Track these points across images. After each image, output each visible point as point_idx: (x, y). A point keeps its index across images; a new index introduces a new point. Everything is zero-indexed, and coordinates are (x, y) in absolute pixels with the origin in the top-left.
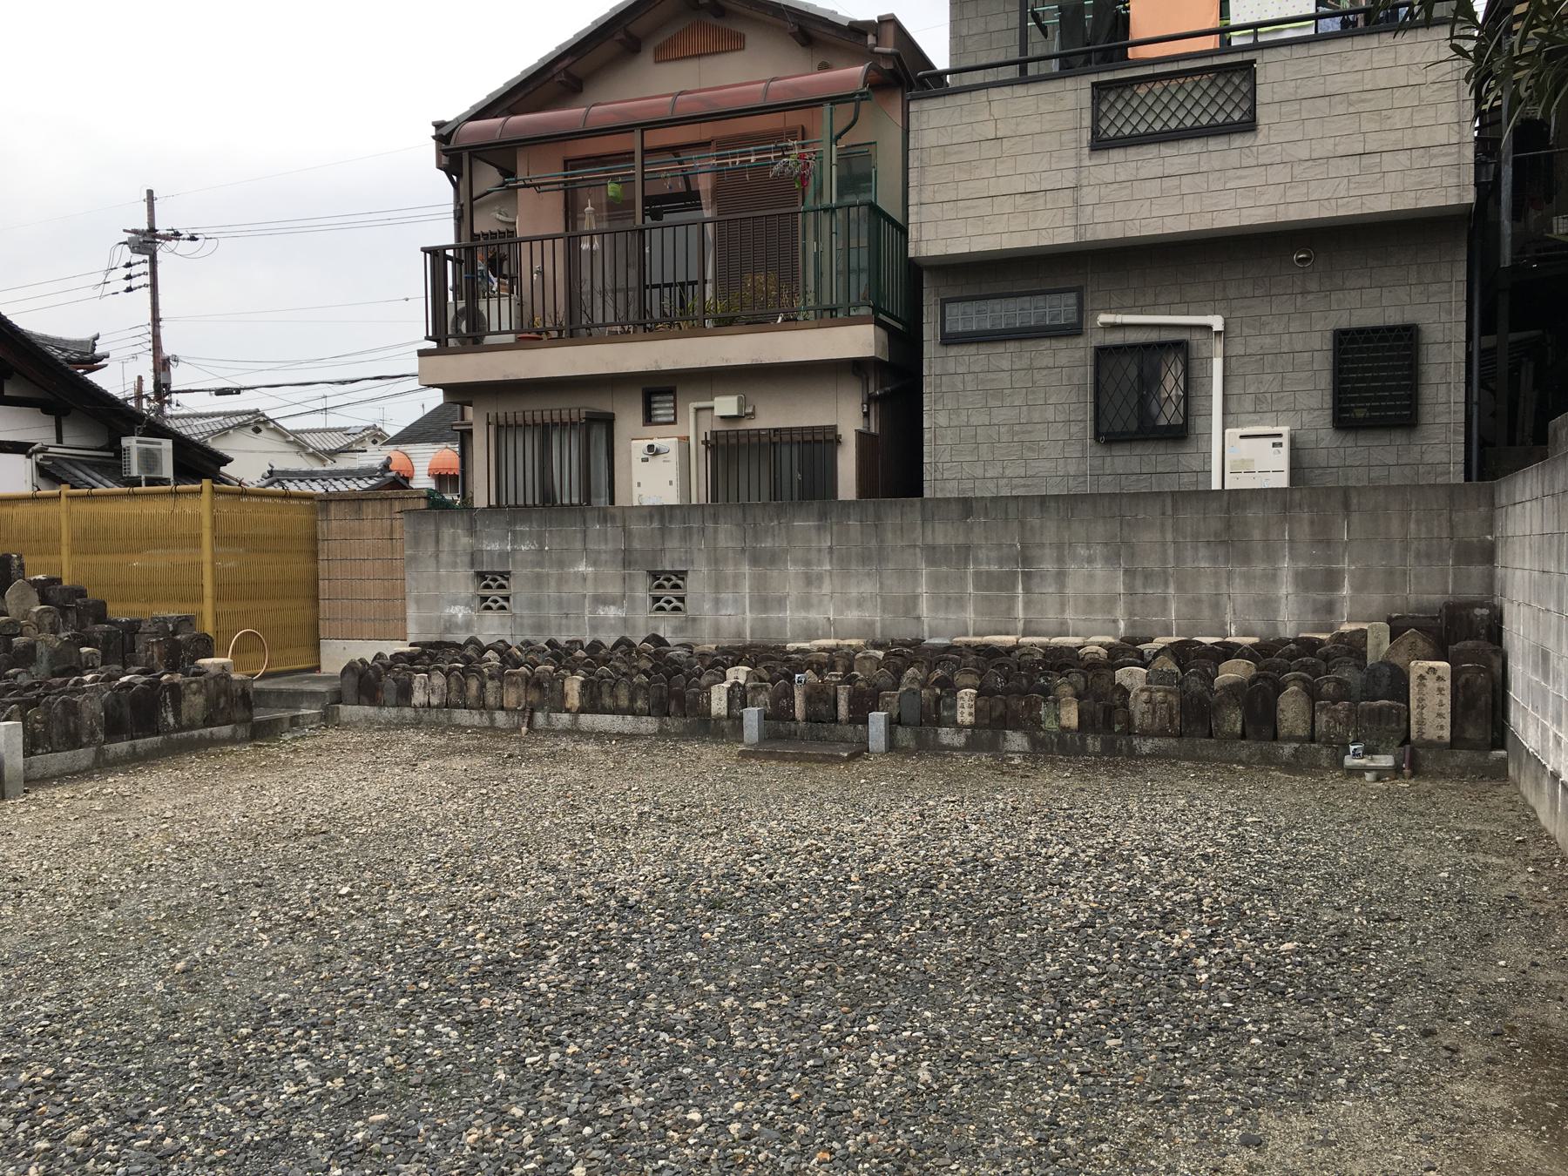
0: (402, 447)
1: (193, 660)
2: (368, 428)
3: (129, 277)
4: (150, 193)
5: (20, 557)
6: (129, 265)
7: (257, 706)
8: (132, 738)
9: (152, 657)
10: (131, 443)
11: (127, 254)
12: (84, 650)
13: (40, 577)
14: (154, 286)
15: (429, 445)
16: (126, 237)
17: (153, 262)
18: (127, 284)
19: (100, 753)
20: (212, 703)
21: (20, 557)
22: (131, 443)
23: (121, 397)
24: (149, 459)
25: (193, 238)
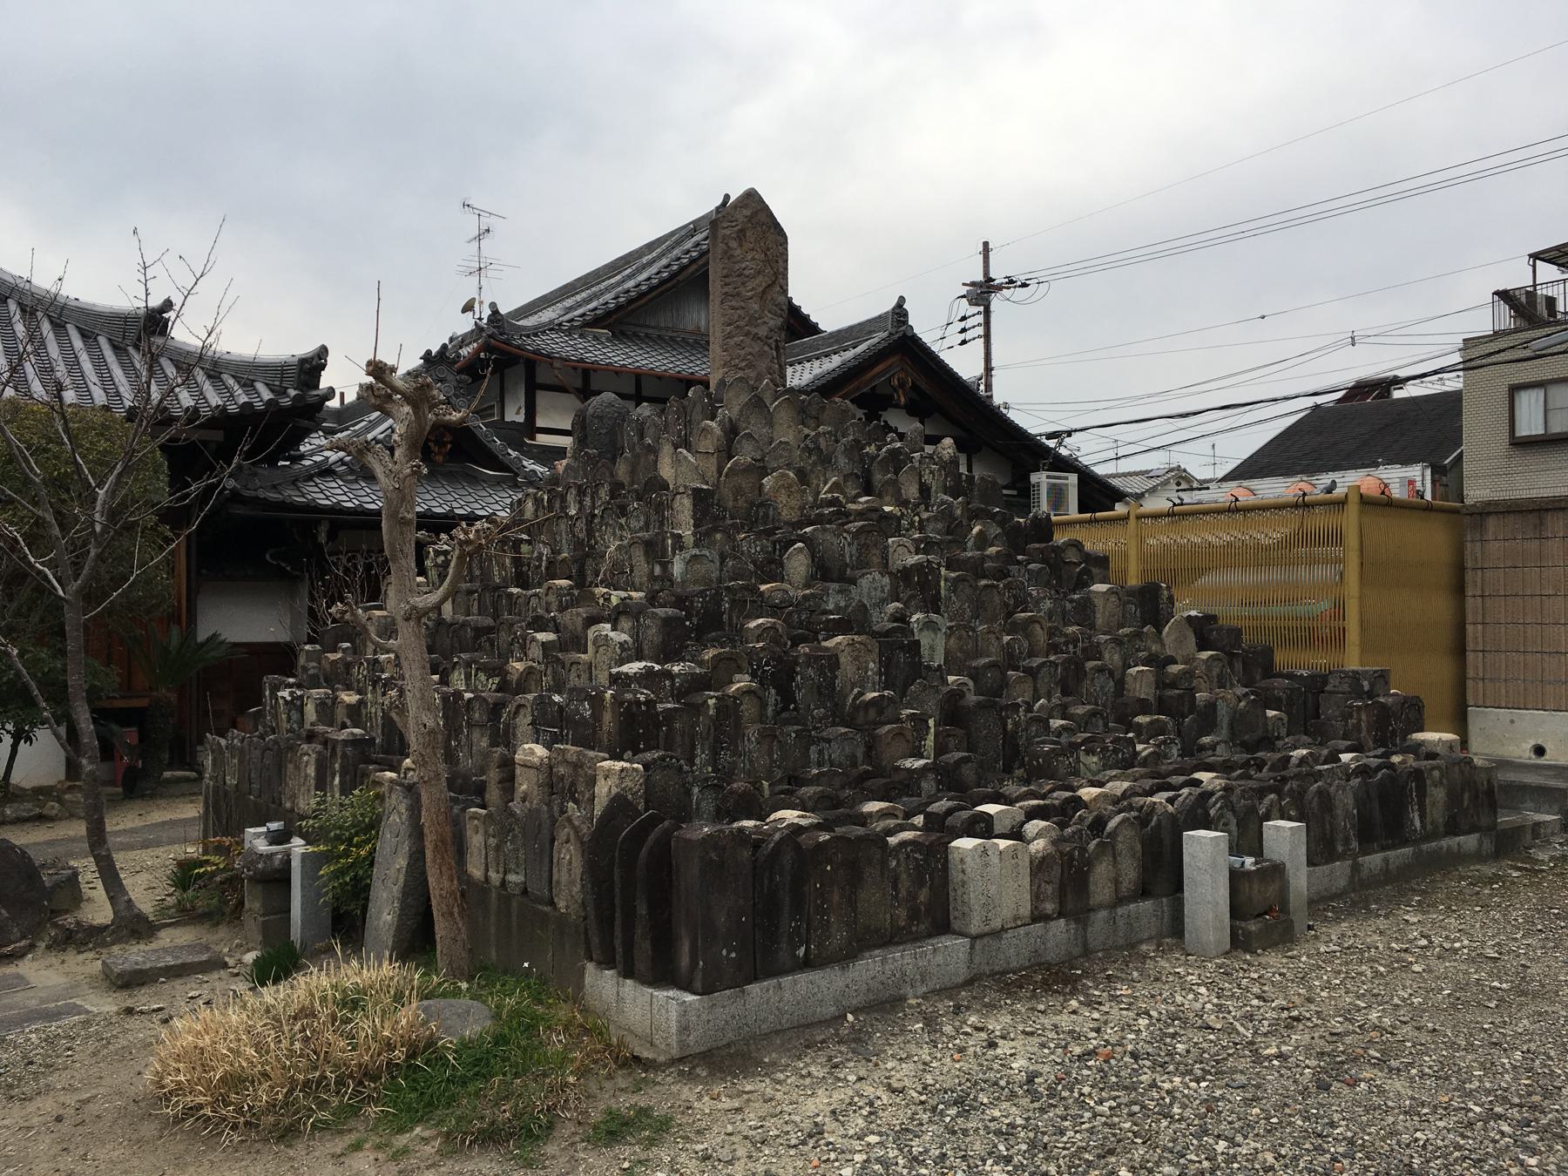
0: (1246, 483)
1: (1404, 739)
2: (1171, 470)
3: (963, 330)
4: (986, 244)
5: (1169, 588)
6: (964, 318)
7: (1502, 807)
8: (1383, 849)
9: (1358, 727)
10: (1041, 479)
11: (965, 307)
12: (1271, 713)
13: (1193, 613)
14: (987, 337)
15: (1281, 479)
16: (964, 290)
17: (987, 313)
18: (962, 336)
19: (1356, 868)
20: (1454, 797)
21: (1169, 588)
22: (1041, 479)
23: (1032, 431)
24: (1057, 496)
25: (1024, 285)
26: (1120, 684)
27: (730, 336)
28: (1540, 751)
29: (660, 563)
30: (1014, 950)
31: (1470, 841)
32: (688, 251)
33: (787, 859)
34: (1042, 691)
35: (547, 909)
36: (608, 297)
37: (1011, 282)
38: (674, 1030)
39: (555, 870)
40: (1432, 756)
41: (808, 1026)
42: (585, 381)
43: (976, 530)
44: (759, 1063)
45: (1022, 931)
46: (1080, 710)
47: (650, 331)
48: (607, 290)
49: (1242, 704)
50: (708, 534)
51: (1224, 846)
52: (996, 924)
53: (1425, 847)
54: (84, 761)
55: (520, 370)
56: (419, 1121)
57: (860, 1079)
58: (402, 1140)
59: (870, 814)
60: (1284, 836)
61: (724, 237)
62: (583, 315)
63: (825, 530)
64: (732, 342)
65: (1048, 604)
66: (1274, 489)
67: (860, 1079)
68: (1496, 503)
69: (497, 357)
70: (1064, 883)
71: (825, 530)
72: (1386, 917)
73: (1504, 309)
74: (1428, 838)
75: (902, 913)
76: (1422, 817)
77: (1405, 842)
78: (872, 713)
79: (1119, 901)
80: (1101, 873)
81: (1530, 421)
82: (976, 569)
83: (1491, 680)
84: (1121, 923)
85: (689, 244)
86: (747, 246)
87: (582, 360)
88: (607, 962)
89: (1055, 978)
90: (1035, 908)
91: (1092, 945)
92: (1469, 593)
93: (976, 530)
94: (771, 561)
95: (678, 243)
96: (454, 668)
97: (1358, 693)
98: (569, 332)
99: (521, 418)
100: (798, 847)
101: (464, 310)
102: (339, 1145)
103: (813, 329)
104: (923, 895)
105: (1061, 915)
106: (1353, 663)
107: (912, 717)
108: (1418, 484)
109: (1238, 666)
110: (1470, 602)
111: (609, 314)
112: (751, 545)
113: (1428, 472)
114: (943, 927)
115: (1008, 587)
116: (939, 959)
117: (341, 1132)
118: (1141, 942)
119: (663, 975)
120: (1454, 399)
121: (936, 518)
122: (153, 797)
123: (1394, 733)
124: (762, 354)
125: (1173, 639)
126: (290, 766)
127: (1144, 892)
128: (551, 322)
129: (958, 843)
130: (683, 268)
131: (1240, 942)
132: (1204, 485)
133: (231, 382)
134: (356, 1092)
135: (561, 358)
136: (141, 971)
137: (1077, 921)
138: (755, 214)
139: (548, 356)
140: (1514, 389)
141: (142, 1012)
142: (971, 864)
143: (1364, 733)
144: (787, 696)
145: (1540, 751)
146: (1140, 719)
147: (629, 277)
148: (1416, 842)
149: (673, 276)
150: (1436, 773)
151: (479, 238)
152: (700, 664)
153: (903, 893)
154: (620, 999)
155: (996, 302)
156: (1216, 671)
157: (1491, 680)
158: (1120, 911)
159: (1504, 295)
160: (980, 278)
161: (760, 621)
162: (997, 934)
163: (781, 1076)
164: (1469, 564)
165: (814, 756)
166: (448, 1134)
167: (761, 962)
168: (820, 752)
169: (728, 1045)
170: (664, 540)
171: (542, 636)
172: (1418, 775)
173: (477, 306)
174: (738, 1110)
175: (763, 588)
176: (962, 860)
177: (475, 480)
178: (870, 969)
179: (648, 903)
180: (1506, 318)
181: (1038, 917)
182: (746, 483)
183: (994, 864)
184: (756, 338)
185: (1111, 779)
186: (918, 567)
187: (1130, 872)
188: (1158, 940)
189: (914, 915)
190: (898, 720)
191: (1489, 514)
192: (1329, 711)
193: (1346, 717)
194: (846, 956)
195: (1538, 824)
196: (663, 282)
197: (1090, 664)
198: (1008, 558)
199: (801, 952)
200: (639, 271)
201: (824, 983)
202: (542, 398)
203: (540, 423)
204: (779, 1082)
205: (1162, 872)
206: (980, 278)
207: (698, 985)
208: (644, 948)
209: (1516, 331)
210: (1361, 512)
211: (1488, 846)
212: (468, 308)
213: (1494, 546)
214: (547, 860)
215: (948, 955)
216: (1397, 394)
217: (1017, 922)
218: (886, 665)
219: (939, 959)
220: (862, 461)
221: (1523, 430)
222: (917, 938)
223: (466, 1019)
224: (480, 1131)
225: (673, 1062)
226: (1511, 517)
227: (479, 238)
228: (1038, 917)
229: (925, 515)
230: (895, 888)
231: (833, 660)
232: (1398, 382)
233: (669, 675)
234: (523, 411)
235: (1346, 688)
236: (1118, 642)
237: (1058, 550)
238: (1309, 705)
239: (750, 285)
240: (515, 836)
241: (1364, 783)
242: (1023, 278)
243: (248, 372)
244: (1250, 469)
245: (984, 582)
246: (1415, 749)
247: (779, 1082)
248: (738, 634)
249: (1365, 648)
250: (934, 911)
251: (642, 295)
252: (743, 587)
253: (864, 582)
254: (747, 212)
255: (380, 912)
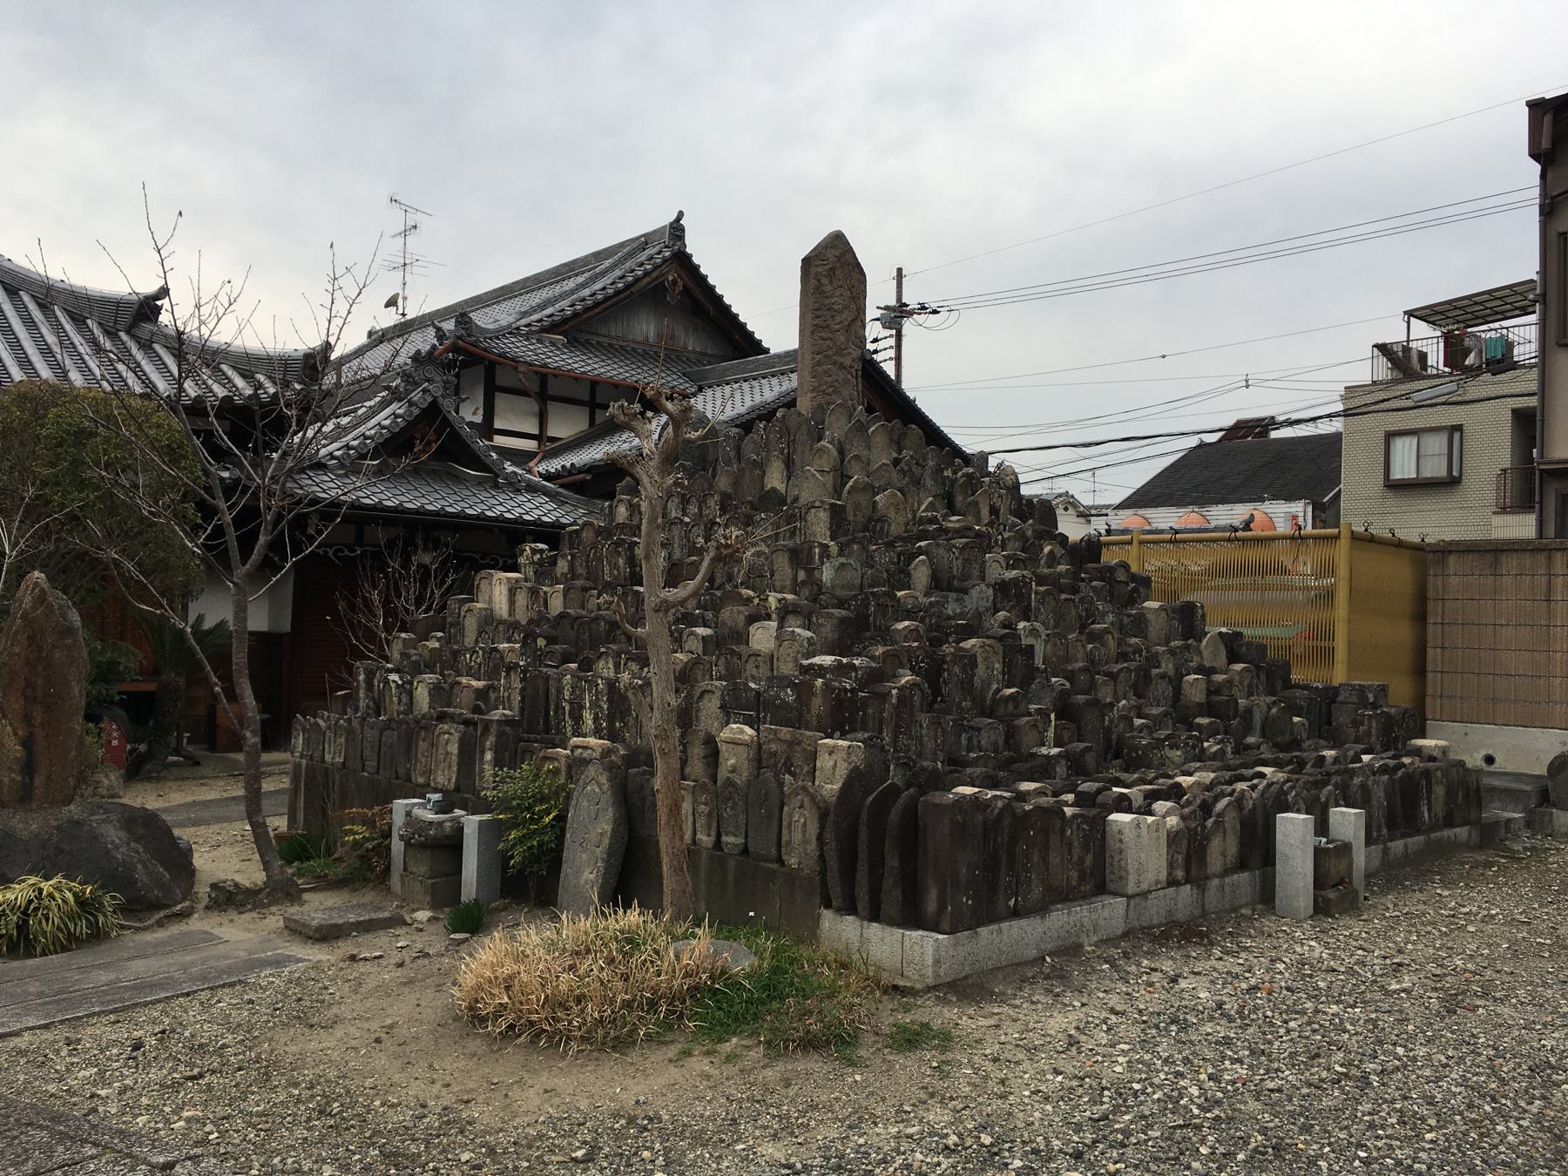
0: (1141, 512)
1: (1404, 744)
4: (900, 270)
8: (1403, 836)
9: (1368, 734)
12: (1296, 719)
13: (1224, 630)
15: (1173, 509)
17: (899, 336)
19: (1386, 851)
20: (1450, 794)
25: (935, 312)
26: (1178, 690)
27: (819, 364)
28: (1490, 760)
29: (806, 569)
30: (1154, 911)
31: (1462, 832)
32: (642, 264)
33: (1007, 822)
34: (1120, 694)
35: (775, 866)
36: (564, 303)
37: (923, 308)
38: (929, 960)
39: (785, 832)
40: (1432, 759)
41: (1018, 965)
42: (545, 390)
43: (1047, 549)
44: (992, 993)
45: (1161, 893)
46: (1155, 711)
47: (602, 339)
48: (563, 296)
49: (1274, 710)
50: (848, 544)
51: (1311, 826)
52: (1145, 886)
53: (1432, 835)
54: (248, 734)
55: (480, 371)
56: (734, 1033)
57: (1083, 1005)
58: (726, 1047)
59: (1028, 792)
60: (1347, 821)
61: (816, 274)
62: (540, 320)
63: (938, 545)
64: (820, 369)
65: (1110, 618)
66: (1165, 518)
67: (1083, 1005)
68: (1458, 543)
69: (461, 354)
70: (1189, 852)
71: (938, 545)
72: (1421, 891)
73: (1383, 362)
74: (1434, 828)
75: (1074, 874)
76: (1429, 810)
77: (1418, 832)
78: (1010, 707)
79: (1227, 872)
80: (1215, 844)
81: (1404, 465)
82: (1053, 581)
83: (1449, 697)
84: (1227, 890)
85: (643, 257)
86: (836, 283)
87: (545, 366)
88: (850, 908)
89: (1187, 933)
90: (1169, 874)
91: (1209, 907)
92: (1431, 620)
93: (1047, 549)
94: (901, 571)
95: (630, 255)
96: (599, 657)
97: (1364, 704)
98: (527, 337)
99: (478, 419)
100: (1014, 814)
101: (387, 305)
102: (672, 1051)
103: (756, 347)
104: (1089, 860)
105: (1187, 881)
106: (1339, 676)
107: (1039, 711)
108: (1301, 520)
109: (1263, 677)
110: (1431, 628)
111: (565, 320)
112: (884, 558)
113: (1310, 509)
114: (1101, 889)
115: (1082, 600)
116: (1106, 913)
117: (665, 1043)
118: (1241, 907)
119: (913, 919)
120: (1336, 438)
121: (1014, 538)
122: (158, 779)
123: (1396, 738)
124: (846, 382)
125: (1209, 650)
126: (422, 745)
127: (1242, 865)
128: (510, 325)
129: (1114, 817)
130: (637, 280)
131: (1322, 909)
132: (1101, 511)
133: (230, 372)
134: (669, 1012)
135: (526, 362)
136: (335, 926)
137: (1199, 887)
138: (843, 254)
139: (513, 360)
140: (1390, 436)
141: (365, 959)
142: (1128, 835)
143: (1373, 739)
144: (936, 691)
145: (1490, 760)
146: (1199, 720)
147: (583, 286)
148: (1426, 832)
149: (628, 286)
150: (1439, 774)
151: (405, 233)
152: (872, 658)
153: (1075, 858)
154: (863, 940)
155: (908, 326)
156: (1246, 683)
157: (1449, 697)
158: (1227, 880)
159: (1383, 348)
160: (893, 302)
161: (907, 623)
162: (1144, 895)
163: (1018, 1002)
164: (1431, 594)
165: (964, 742)
166: (768, 1043)
167: (986, 914)
168: (970, 739)
169: (966, 977)
170: (811, 548)
171: (701, 631)
172: (1427, 774)
173: (400, 301)
174: (997, 1026)
175: (899, 594)
176: (1120, 832)
177: (458, 479)
178: (1060, 920)
179: (889, 857)
180: (1383, 370)
181: (1172, 882)
182: (862, 499)
183: (1141, 833)
184: (842, 367)
185: (1197, 770)
186: (1014, 580)
187: (1232, 847)
188: (1251, 904)
189: (1082, 877)
190: (1030, 714)
191: (1451, 552)
192: (1342, 718)
193: (1356, 724)
194: (1042, 909)
195: (1509, 820)
196: (618, 292)
197: (1155, 671)
198: (1075, 576)
199: (1012, 903)
200: (594, 279)
201: (1029, 929)
202: (501, 401)
203: (498, 425)
204: (1016, 1007)
205: (1258, 848)
206: (893, 302)
207: (945, 926)
208: (892, 896)
209: (1395, 382)
210: (1351, 548)
211: (1475, 838)
212: (392, 303)
213: (1454, 581)
214: (775, 823)
215: (1110, 912)
216: (1274, 435)
217: (1159, 887)
218: (1008, 666)
219: (1106, 913)
220: (944, 484)
221: (1397, 474)
222: (1085, 897)
223: (741, 960)
224: (801, 1039)
225: (929, 989)
226: (1470, 556)
227: (405, 233)
228: (1172, 882)
229: (1006, 535)
230: (1070, 853)
231: (970, 661)
232: (1268, 424)
233: (853, 667)
234: (481, 412)
235: (1354, 699)
236: (1172, 652)
237: (1111, 569)
238: (1324, 710)
239: (838, 319)
240: (735, 804)
241: (1391, 780)
242: (934, 306)
243: (248, 364)
244: (1142, 498)
245: (1064, 596)
246: (1418, 752)
247: (1016, 1007)
248: (886, 635)
249: (1351, 666)
250: (1098, 874)
251: (597, 304)
252: (885, 593)
253: (974, 592)
254: (837, 253)
255: (579, 872)
